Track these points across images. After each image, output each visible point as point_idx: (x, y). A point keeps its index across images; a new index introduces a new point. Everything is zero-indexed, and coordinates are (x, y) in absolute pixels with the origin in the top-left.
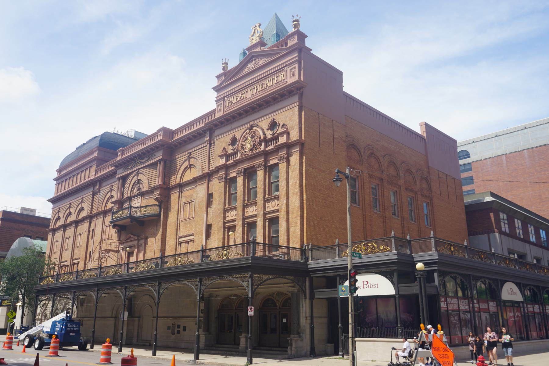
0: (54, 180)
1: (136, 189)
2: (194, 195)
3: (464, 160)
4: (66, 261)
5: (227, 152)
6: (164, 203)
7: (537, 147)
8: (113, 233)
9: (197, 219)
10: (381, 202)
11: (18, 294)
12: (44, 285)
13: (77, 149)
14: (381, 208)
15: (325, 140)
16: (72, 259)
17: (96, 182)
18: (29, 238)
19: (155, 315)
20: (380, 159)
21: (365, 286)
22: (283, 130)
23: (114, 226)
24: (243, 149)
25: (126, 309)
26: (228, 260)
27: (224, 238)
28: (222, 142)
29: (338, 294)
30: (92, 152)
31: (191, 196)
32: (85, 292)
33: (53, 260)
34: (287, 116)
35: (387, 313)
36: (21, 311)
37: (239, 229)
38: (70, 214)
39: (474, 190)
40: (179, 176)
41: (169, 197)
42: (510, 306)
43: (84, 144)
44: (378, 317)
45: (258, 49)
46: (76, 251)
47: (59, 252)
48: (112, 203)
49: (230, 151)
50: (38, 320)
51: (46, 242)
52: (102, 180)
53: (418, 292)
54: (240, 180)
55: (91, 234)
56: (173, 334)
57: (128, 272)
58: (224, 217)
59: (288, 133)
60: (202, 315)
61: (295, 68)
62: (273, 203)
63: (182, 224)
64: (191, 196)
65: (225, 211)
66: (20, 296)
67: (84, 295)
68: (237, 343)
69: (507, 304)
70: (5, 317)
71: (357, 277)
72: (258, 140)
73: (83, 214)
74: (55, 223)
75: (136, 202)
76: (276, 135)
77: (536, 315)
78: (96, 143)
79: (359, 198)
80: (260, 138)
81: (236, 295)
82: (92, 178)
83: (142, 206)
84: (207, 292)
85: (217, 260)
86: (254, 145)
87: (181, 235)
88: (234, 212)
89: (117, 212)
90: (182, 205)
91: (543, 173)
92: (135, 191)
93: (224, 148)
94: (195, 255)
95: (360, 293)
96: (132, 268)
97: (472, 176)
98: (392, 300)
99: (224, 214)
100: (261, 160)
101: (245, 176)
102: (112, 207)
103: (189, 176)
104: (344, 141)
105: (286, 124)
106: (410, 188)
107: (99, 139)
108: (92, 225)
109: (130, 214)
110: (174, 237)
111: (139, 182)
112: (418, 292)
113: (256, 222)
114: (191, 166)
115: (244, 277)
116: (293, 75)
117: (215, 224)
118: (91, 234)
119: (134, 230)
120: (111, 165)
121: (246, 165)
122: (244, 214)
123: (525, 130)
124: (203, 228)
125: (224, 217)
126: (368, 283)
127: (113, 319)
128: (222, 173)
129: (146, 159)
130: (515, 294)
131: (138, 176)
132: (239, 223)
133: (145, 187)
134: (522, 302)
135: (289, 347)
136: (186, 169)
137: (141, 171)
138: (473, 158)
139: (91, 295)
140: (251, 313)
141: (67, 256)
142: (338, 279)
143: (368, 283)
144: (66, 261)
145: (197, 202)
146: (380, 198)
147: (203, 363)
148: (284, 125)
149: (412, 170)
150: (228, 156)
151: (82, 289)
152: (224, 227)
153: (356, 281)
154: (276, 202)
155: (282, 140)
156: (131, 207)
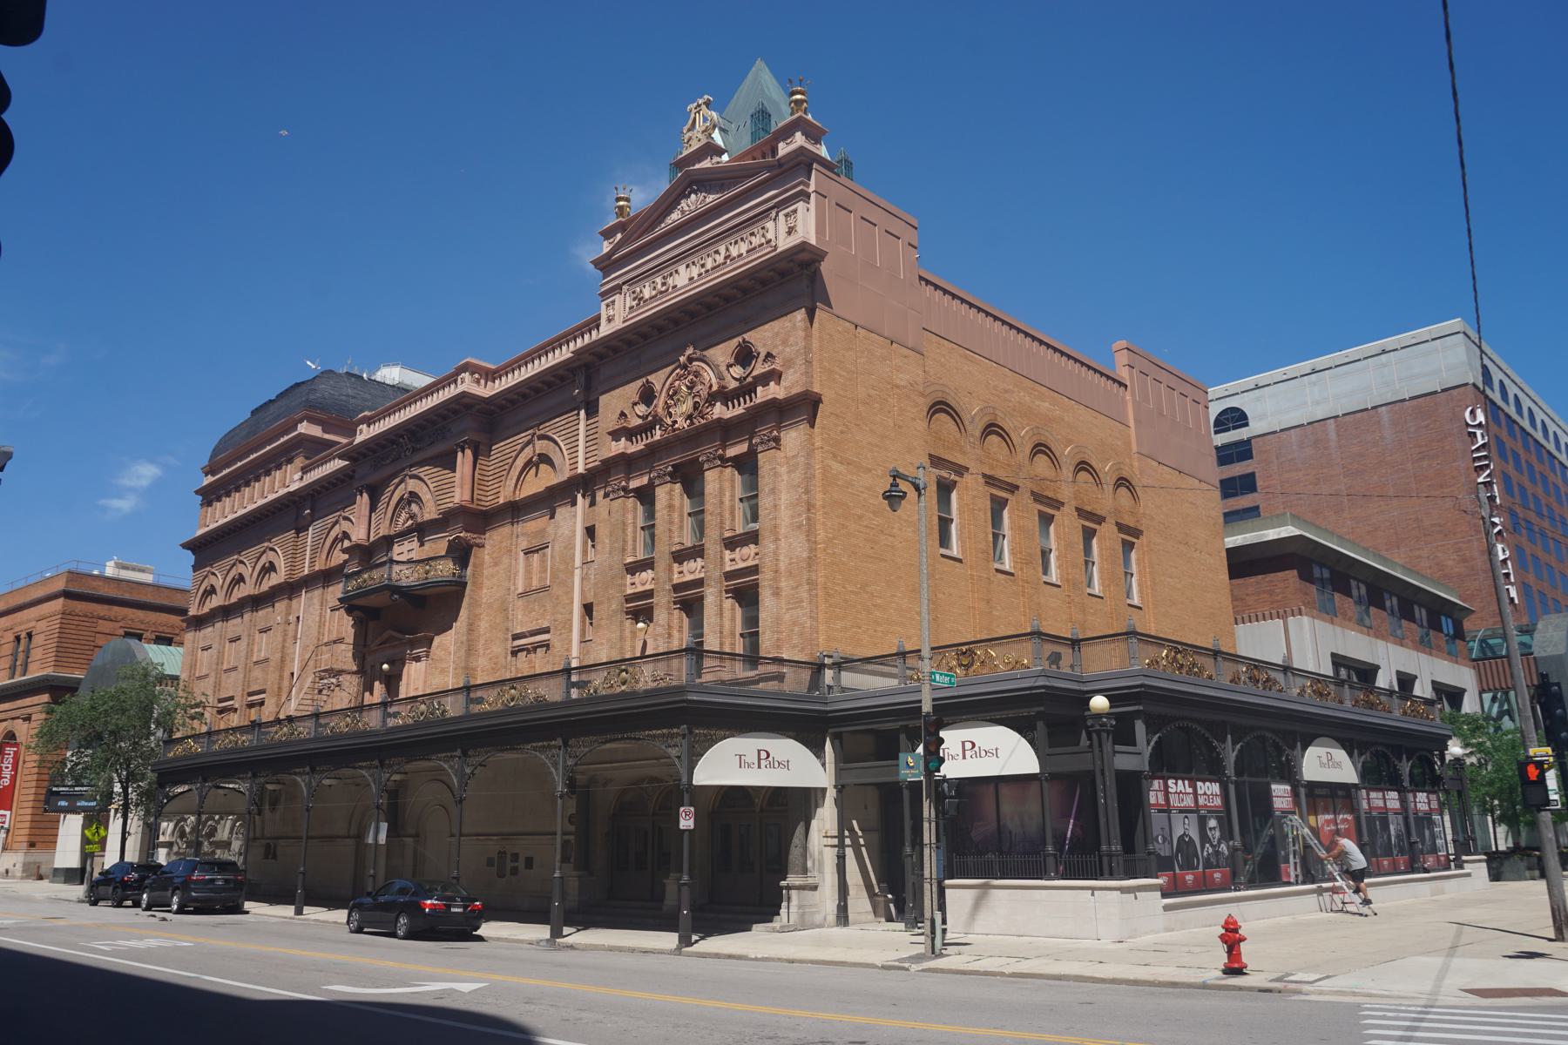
1: (404, 515)
2: (550, 530)
3: (1232, 432)
4: (232, 698)
7: (1412, 398)
8: (345, 625)
9: (555, 590)
11: (110, 782)
12: (176, 759)
13: (253, 413)
15: (872, 392)
19: (455, 831)
21: (968, 754)
22: (767, 367)
23: (349, 611)
24: (670, 415)
25: (382, 816)
26: (633, 695)
28: (618, 402)
29: (897, 773)
31: (543, 531)
32: (280, 776)
34: (777, 334)
35: (1019, 815)
39: (1257, 508)
40: (511, 482)
42: (1325, 796)
44: (1000, 829)
45: (706, 164)
48: (344, 551)
50: (164, 845)
51: (180, 649)
52: (319, 493)
56: (501, 875)
57: (384, 722)
60: (572, 828)
62: (745, 550)
64: (543, 531)
66: (117, 788)
67: (278, 783)
68: (658, 896)
69: (1318, 792)
70: (79, 838)
71: (942, 734)
72: (704, 394)
75: (405, 550)
76: (749, 379)
77: (1391, 817)
81: (653, 779)
83: (411, 562)
84: (582, 773)
85: (618, 690)
89: (358, 573)
91: (1425, 463)
92: (401, 520)
94: (552, 682)
95: (952, 769)
96: (395, 715)
97: (1253, 474)
98: (1035, 786)
102: (346, 562)
104: (922, 395)
113: (701, 598)
115: (672, 736)
117: (601, 603)
119: (395, 621)
120: (341, 457)
121: (677, 458)
123: (1383, 357)
124: (571, 613)
126: (974, 745)
127: (351, 842)
130: (1339, 765)
133: (430, 512)
134: (1354, 785)
135: (784, 904)
136: (529, 464)
138: (1255, 427)
139: (296, 784)
142: (903, 737)
143: (974, 745)
144: (232, 698)
145: (557, 548)
147: (572, 947)
148: (769, 355)
151: (270, 766)
153: (942, 741)
154: (751, 549)
156: (392, 561)
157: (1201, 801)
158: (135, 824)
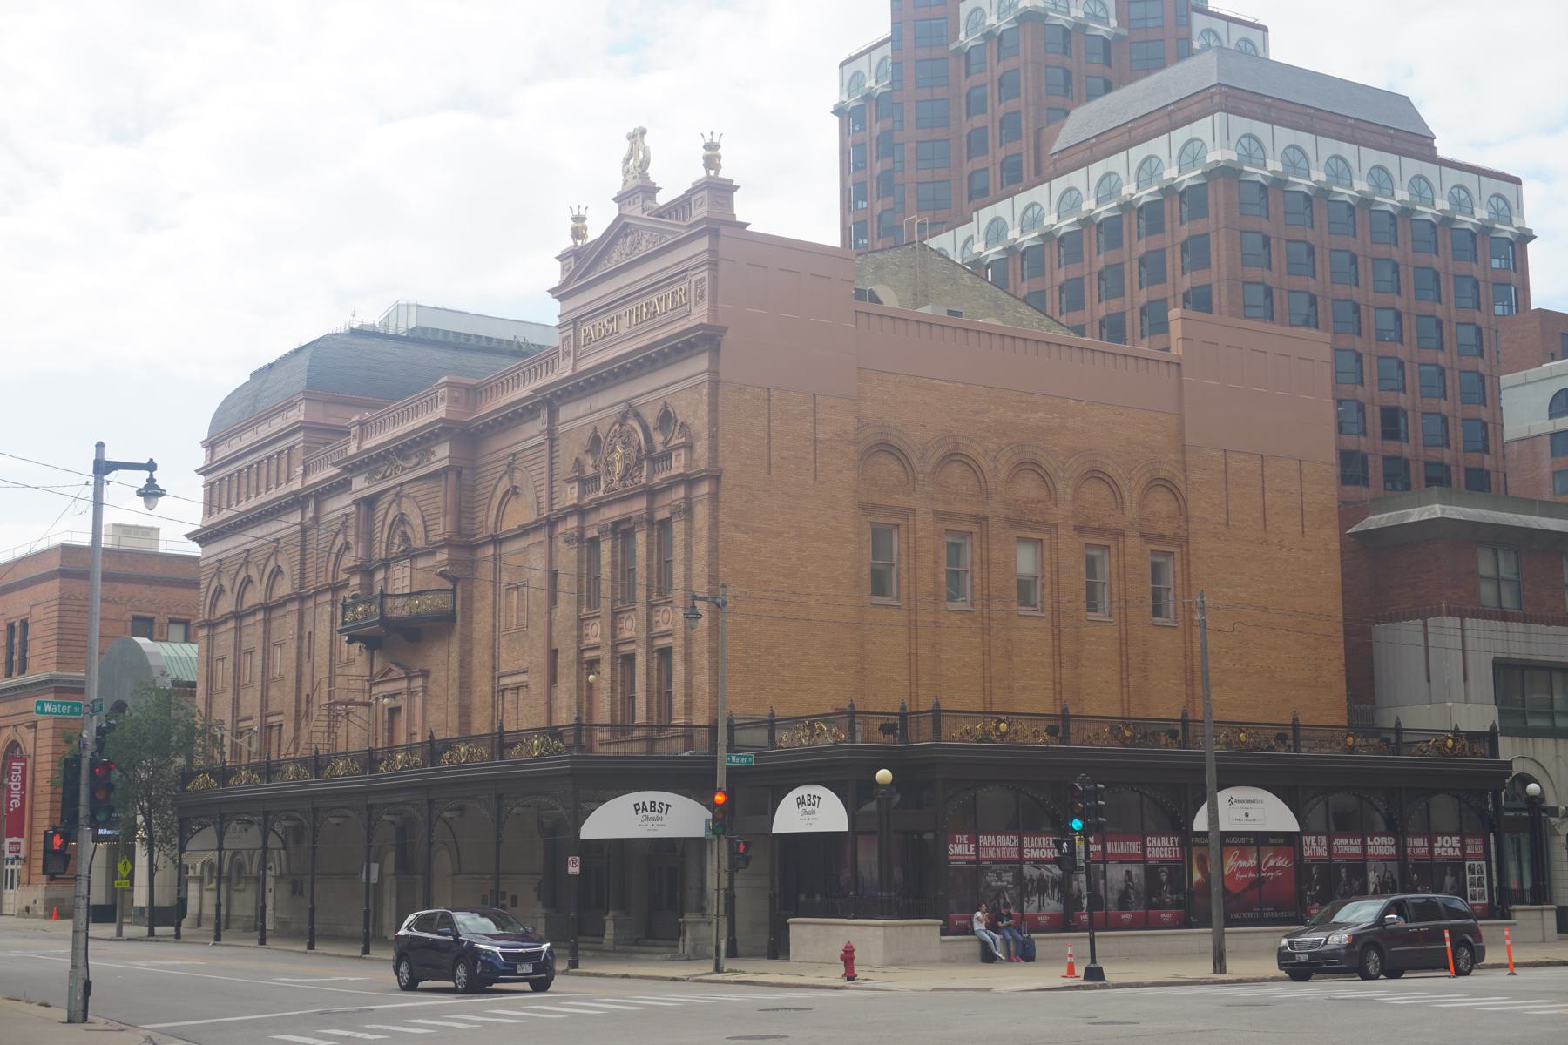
0: (199, 471)
5: (582, 470)
6: (459, 578)
10: (977, 580)
14: (978, 596)
16: (265, 714)
17: (306, 498)
18: (146, 640)
20: (982, 462)
27: (579, 689)
30: (290, 405)
33: (216, 716)
36: (146, 859)
37: (605, 669)
38: (248, 581)
41: (472, 566)
43: (271, 366)
46: (273, 692)
47: (230, 690)
49: (590, 471)
53: (91, 926)
54: (605, 548)
55: (304, 639)
58: (580, 638)
59: (689, 447)
61: (702, 279)
63: (503, 641)
65: (581, 622)
66: (140, 819)
73: (284, 588)
74: (213, 605)
75: (401, 579)
78: (297, 380)
79: (899, 582)
80: (639, 450)
82: (296, 485)
86: (627, 468)
87: (504, 669)
90: (503, 590)
93: (577, 460)
99: (580, 629)
100: (639, 505)
101: (614, 539)
103: (510, 524)
105: (688, 422)
106: (1097, 524)
107: (307, 353)
108: (308, 620)
109: (382, 613)
110: (489, 673)
111: (402, 519)
112: (91, 926)
114: (514, 491)
116: (701, 297)
118: (304, 639)
122: (613, 636)
125: (580, 638)
128: (572, 523)
129: (414, 461)
131: (399, 505)
132: (605, 654)
137: (407, 490)
140: (574, 869)
141: (251, 701)
146: (977, 568)
149: (1110, 471)
150: (585, 483)
152: (580, 661)
155: (678, 465)
157: (983, 854)
158: (678, 719)
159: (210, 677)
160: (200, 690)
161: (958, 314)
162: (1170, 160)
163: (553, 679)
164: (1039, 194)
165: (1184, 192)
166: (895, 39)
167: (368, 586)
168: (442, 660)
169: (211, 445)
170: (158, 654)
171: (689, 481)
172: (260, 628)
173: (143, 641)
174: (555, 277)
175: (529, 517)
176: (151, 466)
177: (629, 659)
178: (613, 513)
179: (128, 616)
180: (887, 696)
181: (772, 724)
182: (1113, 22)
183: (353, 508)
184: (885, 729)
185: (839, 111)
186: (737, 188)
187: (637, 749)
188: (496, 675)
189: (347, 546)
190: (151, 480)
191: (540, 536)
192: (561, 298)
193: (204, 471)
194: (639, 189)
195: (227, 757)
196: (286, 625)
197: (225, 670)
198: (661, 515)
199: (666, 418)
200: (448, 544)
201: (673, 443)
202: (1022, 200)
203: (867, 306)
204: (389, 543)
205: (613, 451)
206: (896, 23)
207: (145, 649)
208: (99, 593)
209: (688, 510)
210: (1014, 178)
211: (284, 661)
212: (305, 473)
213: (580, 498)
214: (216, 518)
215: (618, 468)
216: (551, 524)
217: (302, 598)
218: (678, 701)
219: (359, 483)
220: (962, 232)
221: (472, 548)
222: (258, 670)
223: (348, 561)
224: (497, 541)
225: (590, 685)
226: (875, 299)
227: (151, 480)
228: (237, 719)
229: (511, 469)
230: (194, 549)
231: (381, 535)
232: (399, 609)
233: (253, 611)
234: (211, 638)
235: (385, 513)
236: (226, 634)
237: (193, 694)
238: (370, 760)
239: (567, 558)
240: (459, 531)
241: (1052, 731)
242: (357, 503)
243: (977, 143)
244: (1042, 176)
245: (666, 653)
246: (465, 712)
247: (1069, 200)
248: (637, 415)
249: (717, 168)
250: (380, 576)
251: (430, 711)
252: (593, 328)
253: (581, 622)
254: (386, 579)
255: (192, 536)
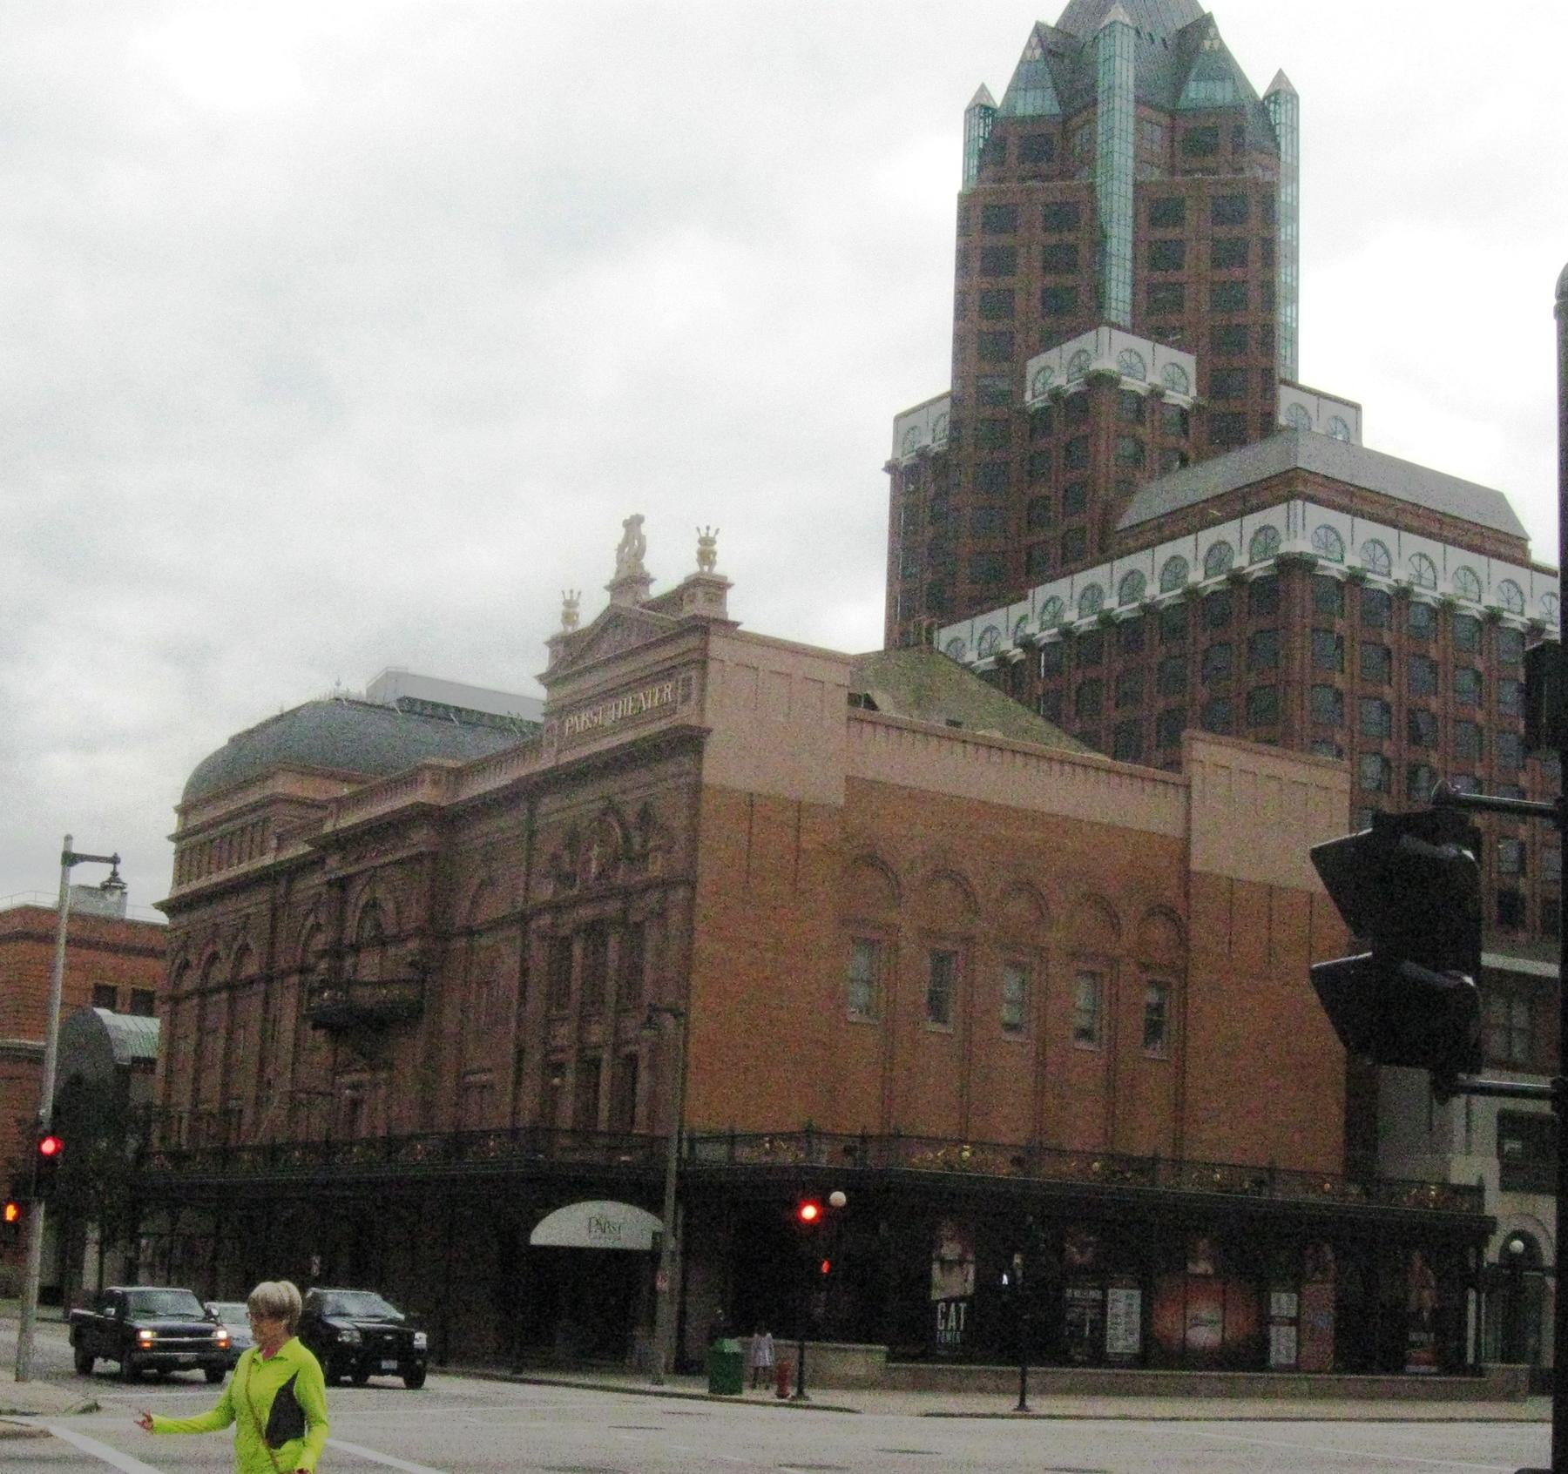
16: (226, 1096)
65: (549, 1022)
73: (252, 968)
75: (370, 966)
82: (268, 860)
88: (564, 1030)
100: (613, 907)
111: (373, 905)
118: (270, 1022)
128: (546, 920)
132: (570, 1058)
150: (566, 879)
159: (170, 1056)
160: (160, 1069)
161: (957, 724)
162: (1240, 544)
163: (518, 1083)
164: (1099, 575)
165: (1254, 582)
166: (955, 398)
167: (336, 971)
168: (408, 1051)
169: (184, 811)
170: (118, 1028)
171: (666, 884)
172: (224, 1006)
173: (103, 1013)
174: (542, 663)
175: (503, 910)
176: (115, 860)
177: (596, 1064)
178: (586, 913)
179: (91, 984)
180: (863, 1117)
181: (732, 1139)
182: (1193, 391)
183: (324, 889)
184: (848, 1151)
185: (891, 468)
186: (729, 586)
187: (597, 1157)
188: (460, 1076)
189: (317, 927)
190: (114, 874)
191: (514, 931)
192: (549, 686)
193: (176, 838)
194: (630, 580)
195: (183, 1141)
196: (252, 1007)
197: (187, 1047)
198: (636, 917)
199: (645, 816)
200: (420, 932)
201: (651, 844)
202: (1082, 579)
203: (861, 711)
204: (360, 927)
205: (589, 849)
206: (957, 376)
207: (106, 1021)
208: (36, 1282)
209: (662, 915)
210: (1071, 559)
211: (248, 1043)
212: (279, 849)
213: (555, 892)
214: (186, 889)
215: (594, 868)
216: (523, 919)
217: (269, 980)
218: (641, 1111)
219: (334, 865)
220: (1017, 610)
221: (445, 937)
222: (220, 1052)
223: (320, 941)
224: (470, 932)
225: (555, 1089)
226: (871, 705)
227: (114, 874)
228: (196, 1101)
229: (487, 860)
230: (162, 918)
231: (352, 923)
232: (364, 997)
233: (218, 990)
234: (174, 1012)
235: (359, 895)
236: (190, 1007)
237: (153, 1071)
238: (329, 1147)
239: (540, 954)
240: (432, 920)
241: (1017, 1161)
242: (329, 883)
243: (1035, 514)
244: (1105, 554)
245: (632, 1060)
246: (427, 1106)
247: (1132, 584)
248: (617, 812)
249: (712, 564)
250: (349, 962)
251: (391, 1103)
252: (580, 721)
253: (549, 1022)
254: (355, 966)
255: (162, 906)
